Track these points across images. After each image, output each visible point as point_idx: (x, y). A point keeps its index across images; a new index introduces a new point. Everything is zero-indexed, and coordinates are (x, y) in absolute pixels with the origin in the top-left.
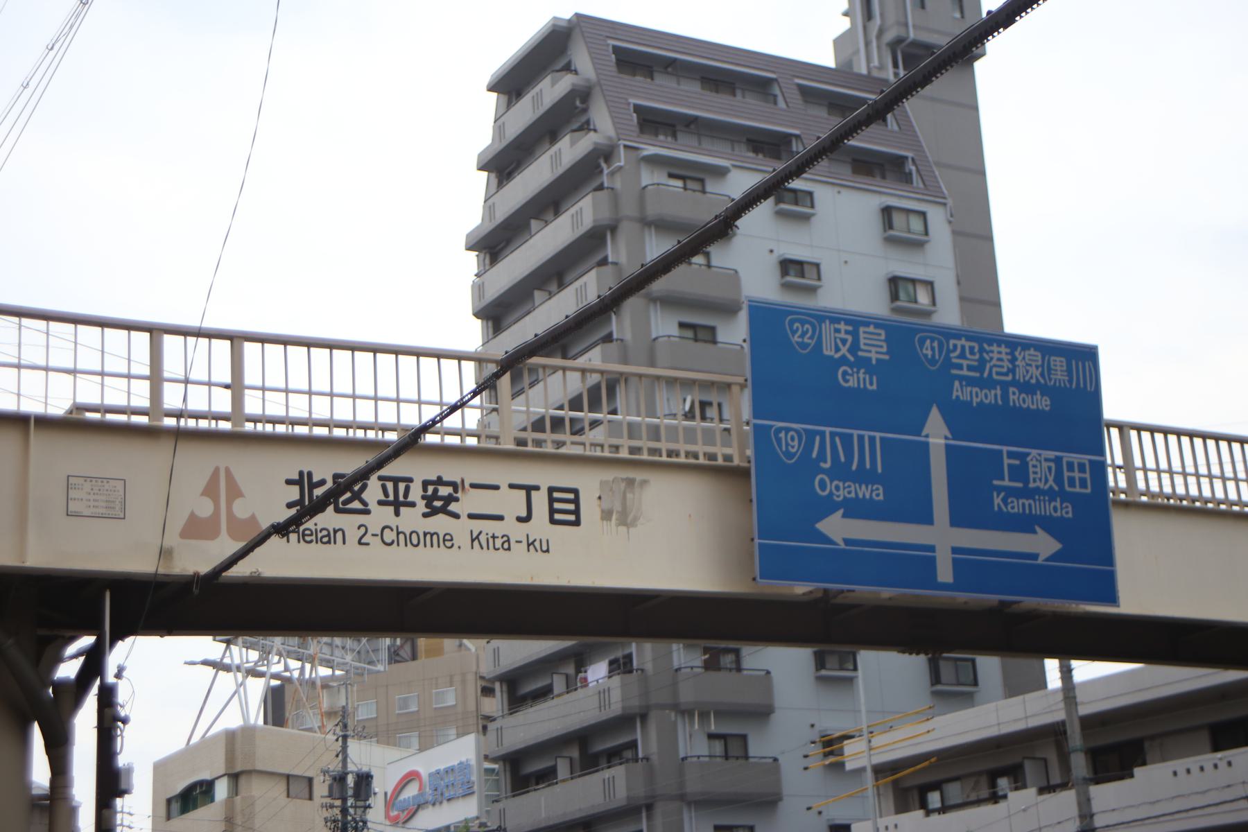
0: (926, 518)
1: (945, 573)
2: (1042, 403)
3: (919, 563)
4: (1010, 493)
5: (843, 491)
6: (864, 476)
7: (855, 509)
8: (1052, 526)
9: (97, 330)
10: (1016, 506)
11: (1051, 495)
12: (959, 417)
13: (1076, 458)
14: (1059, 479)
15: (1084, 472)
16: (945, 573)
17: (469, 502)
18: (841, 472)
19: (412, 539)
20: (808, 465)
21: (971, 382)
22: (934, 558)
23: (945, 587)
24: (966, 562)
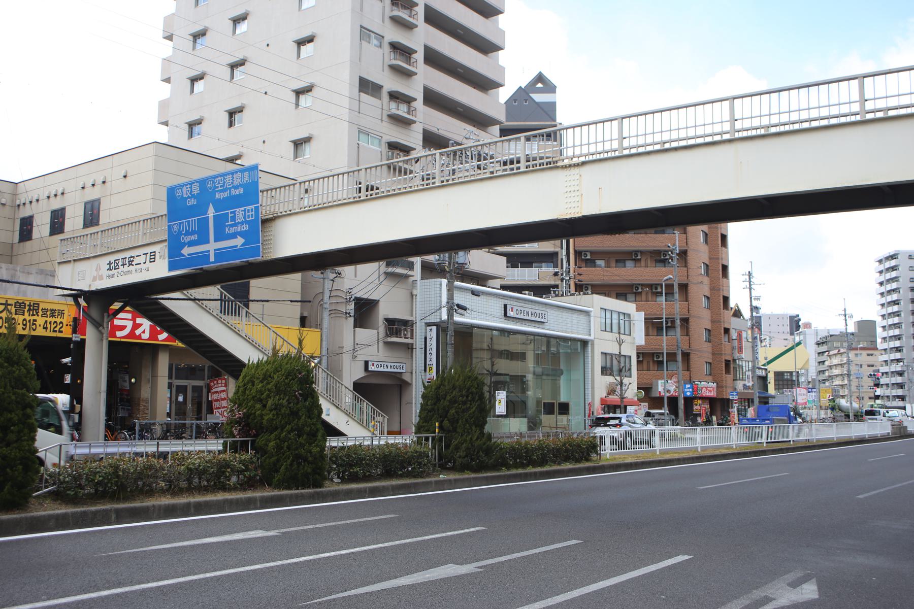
0: (217, 240)
1: (212, 259)
2: (241, 191)
3: (205, 256)
4: (232, 226)
5: (187, 239)
6: (193, 233)
7: (191, 244)
8: (241, 234)
9: (826, 86)
10: (232, 230)
11: (242, 223)
12: (218, 205)
13: (249, 207)
14: (245, 218)
15: (519, 138)
16: (212, 259)
17: (136, 261)
18: (188, 233)
19: (125, 273)
20: (180, 233)
21: (221, 191)
22: (553, 105)
23: (212, 263)
24: (219, 254)
